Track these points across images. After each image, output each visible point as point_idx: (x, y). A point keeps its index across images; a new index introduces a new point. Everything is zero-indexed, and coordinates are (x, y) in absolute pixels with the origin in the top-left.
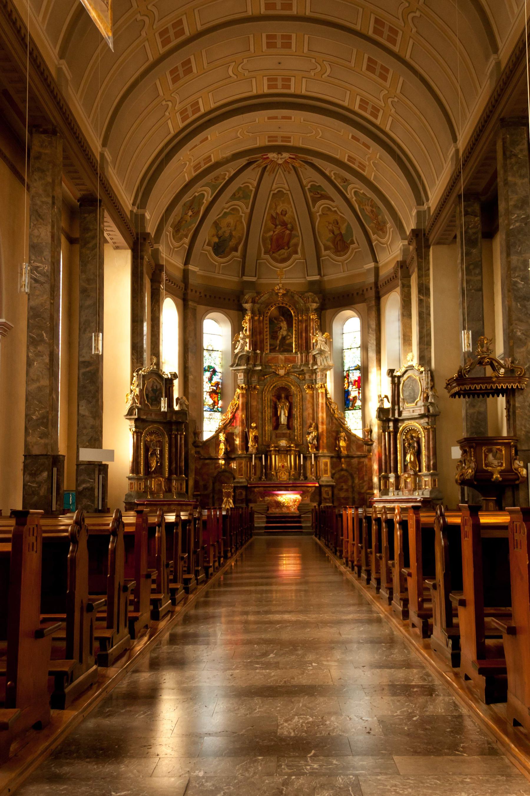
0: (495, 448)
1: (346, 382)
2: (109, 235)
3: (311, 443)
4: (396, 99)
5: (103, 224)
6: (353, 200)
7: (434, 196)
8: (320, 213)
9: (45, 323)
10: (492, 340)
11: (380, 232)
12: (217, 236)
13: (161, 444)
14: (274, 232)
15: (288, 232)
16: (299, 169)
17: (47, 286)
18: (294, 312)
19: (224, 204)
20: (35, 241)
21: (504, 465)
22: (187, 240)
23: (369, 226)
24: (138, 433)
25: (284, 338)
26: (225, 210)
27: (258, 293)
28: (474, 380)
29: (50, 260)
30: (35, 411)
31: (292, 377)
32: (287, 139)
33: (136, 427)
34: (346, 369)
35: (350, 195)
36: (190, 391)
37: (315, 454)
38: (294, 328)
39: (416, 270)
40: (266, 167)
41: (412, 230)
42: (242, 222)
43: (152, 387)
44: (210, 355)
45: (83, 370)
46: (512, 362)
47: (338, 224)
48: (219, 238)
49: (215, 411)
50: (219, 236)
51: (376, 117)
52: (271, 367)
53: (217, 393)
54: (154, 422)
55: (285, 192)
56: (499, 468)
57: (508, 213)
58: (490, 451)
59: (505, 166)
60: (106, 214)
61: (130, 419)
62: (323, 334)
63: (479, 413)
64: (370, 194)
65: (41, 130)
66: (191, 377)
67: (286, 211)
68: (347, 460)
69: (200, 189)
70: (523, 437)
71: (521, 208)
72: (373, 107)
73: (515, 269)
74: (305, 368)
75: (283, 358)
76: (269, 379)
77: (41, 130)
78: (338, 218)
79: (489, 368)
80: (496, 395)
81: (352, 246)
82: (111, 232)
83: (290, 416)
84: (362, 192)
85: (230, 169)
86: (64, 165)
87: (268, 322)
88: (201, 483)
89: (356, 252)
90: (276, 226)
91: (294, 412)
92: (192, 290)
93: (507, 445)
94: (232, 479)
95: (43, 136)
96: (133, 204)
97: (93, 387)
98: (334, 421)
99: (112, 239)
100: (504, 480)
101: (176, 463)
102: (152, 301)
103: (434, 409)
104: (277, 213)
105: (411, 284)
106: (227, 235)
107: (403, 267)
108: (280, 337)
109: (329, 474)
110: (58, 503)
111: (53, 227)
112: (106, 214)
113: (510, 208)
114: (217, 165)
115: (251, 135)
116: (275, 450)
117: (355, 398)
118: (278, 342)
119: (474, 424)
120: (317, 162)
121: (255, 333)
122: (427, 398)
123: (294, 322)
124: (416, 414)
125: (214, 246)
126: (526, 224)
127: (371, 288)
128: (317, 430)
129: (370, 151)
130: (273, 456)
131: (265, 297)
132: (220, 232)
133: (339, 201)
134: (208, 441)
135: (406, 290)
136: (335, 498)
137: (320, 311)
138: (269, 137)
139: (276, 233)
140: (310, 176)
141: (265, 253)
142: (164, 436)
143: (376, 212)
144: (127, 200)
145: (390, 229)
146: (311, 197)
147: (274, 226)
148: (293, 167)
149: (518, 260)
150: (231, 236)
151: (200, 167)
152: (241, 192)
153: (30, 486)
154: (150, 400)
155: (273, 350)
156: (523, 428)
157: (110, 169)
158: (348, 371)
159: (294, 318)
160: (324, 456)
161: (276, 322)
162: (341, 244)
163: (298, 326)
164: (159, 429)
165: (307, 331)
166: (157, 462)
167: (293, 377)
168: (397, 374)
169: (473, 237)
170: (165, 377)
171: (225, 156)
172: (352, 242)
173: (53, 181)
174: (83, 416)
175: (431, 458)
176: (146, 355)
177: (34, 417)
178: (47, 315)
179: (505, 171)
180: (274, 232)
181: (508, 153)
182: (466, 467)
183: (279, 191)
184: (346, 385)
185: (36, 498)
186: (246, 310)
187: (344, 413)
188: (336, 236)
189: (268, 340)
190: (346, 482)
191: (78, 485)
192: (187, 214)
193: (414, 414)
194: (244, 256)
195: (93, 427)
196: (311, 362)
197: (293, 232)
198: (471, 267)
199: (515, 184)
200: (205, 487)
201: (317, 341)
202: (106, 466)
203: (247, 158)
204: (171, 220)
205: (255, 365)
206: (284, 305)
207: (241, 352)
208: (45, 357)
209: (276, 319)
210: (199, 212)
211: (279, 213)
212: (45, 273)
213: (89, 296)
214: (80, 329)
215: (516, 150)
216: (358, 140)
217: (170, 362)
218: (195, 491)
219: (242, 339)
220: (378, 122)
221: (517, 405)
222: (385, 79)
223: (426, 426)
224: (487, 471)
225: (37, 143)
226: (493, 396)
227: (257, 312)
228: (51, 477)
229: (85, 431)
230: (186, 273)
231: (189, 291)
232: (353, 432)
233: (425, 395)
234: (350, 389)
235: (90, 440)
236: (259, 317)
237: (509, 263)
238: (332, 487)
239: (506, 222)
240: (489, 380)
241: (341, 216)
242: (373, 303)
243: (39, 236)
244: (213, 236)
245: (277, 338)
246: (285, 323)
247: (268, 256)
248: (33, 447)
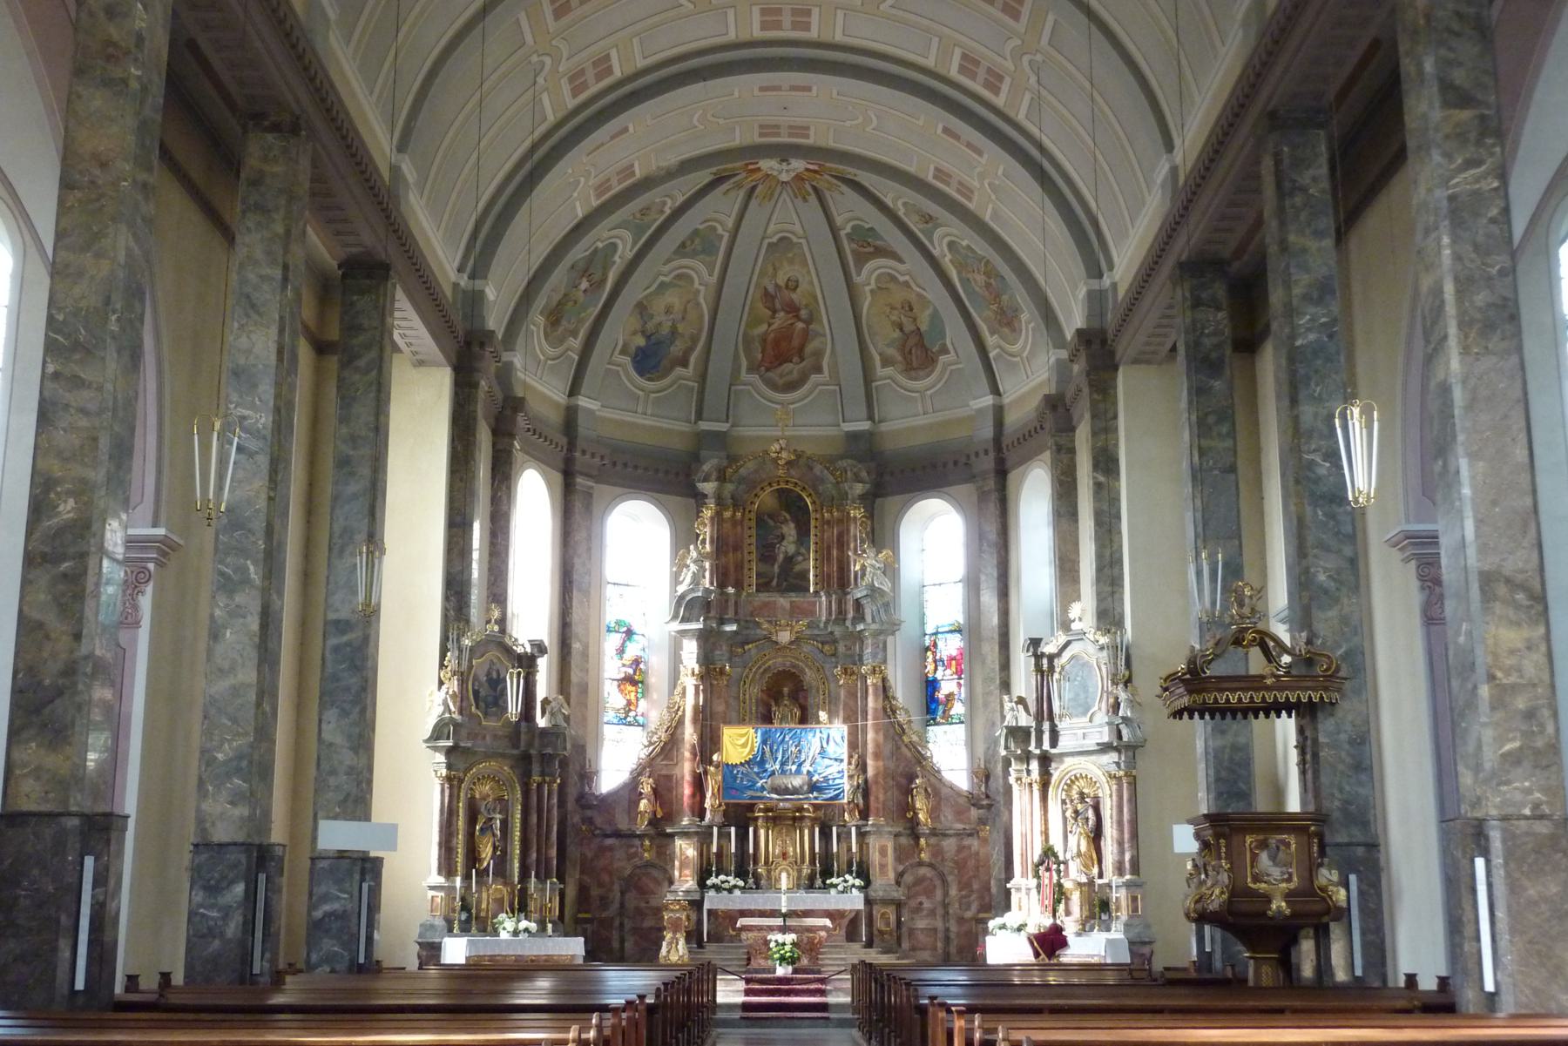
0: (1273, 840)
1: (930, 659)
2: (403, 336)
4: (1039, 57)
5: (392, 314)
6: (947, 261)
7: (1126, 258)
8: (873, 286)
9: (255, 543)
10: (1261, 591)
11: (1006, 330)
12: (643, 332)
13: (503, 804)
16: (827, 194)
17: (263, 461)
18: (813, 503)
19: (659, 265)
20: (242, 361)
21: (1295, 879)
22: (576, 343)
24: (452, 782)
25: (789, 560)
26: (662, 278)
27: (733, 459)
28: (1223, 683)
29: (271, 404)
30: (222, 741)
31: (806, 648)
32: (803, 130)
33: (449, 767)
34: (929, 629)
35: (939, 249)
37: (858, 827)
38: (812, 538)
39: (1087, 416)
40: (753, 188)
41: (1078, 331)
42: (698, 304)
43: (488, 674)
45: (333, 641)
46: (1309, 642)
48: (648, 338)
49: (630, 724)
51: (996, 90)
52: (758, 625)
53: (634, 683)
54: (488, 756)
55: (795, 240)
56: (1284, 885)
57: (1290, 312)
58: (1263, 845)
59: (1281, 211)
60: (400, 294)
61: (436, 749)
62: (879, 552)
63: (1235, 748)
64: (982, 248)
65: (266, 123)
68: (933, 840)
69: (606, 234)
70: (1336, 815)
71: (1320, 301)
72: (989, 71)
73: (1310, 434)
74: (838, 631)
75: (788, 606)
76: (753, 652)
77: (266, 123)
78: (913, 298)
79: (1255, 653)
80: (1273, 714)
81: (943, 359)
82: (409, 327)
84: (964, 243)
85: (676, 192)
86: (313, 194)
87: (753, 524)
88: (595, 892)
90: (774, 312)
93: (1302, 830)
95: (270, 137)
96: (460, 270)
97: (354, 680)
98: (904, 750)
99: (409, 345)
100: (1294, 915)
101: (538, 851)
102: (493, 478)
103: (1133, 732)
104: (777, 286)
105: (1077, 443)
106: (665, 330)
107: (1057, 408)
108: (781, 557)
109: (891, 875)
110: (267, 955)
111: (281, 331)
112: (400, 294)
113: (1295, 302)
114: (647, 184)
115: (721, 121)
116: (767, 819)
117: (950, 697)
118: (776, 569)
119: (1224, 774)
120: (866, 178)
121: (723, 546)
122: (1116, 707)
123: (813, 523)
124: (1091, 743)
126: (1331, 336)
127: (986, 452)
128: (864, 771)
129: (983, 160)
130: (762, 832)
131: (747, 468)
132: (650, 326)
133: (913, 262)
134: (614, 794)
135: (1065, 457)
136: (904, 929)
137: (870, 500)
138: (761, 126)
140: (850, 209)
141: (750, 370)
142: (513, 788)
143: (995, 289)
144: (444, 257)
145: (1028, 323)
146: (853, 251)
148: (815, 189)
149: (1316, 415)
150: (674, 332)
151: (609, 189)
152: (697, 241)
153: (203, 915)
154: (482, 704)
155: (764, 586)
156: (1337, 795)
157: (412, 197)
158: (936, 634)
159: (813, 515)
161: (771, 523)
162: (919, 353)
163: (823, 532)
165: (842, 544)
166: (495, 848)
168: (1049, 648)
169: (1214, 355)
170: (520, 650)
171: (664, 164)
172: (944, 351)
173: (288, 232)
174: (331, 744)
175: (1126, 846)
176: (476, 596)
177: (220, 756)
178: (259, 525)
179: (1282, 224)
181: (1287, 184)
182: (1209, 883)
183: (781, 239)
184: (930, 667)
185: (217, 943)
186: (705, 496)
187: (926, 732)
188: (907, 336)
190: (929, 893)
191: (312, 907)
192: (577, 290)
193: (1087, 742)
194: (703, 377)
195: (351, 771)
196: (851, 615)
198: (1211, 419)
199: (1304, 251)
200: (604, 902)
201: (863, 568)
202: (378, 862)
203: (714, 170)
204: (541, 302)
205: (722, 622)
206: (790, 486)
207: (692, 590)
208: (249, 618)
209: (771, 516)
210: (603, 281)
212: (258, 431)
213: (352, 474)
214: (330, 549)
215: (1305, 178)
216: (957, 137)
217: (530, 615)
218: (579, 911)
219: (695, 562)
220: (1000, 101)
221: (1322, 739)
222: (1016, 16)
223: (1113, 769)
224: (1255, 894)
225: (258, 151)
226: (1267, 716)
227: (730, 501)
228: (251, 894)
229: (332, 781)
230: (570, 419)
231: (577, 454)
232: (947, 776)
233: (1111, 700)
234: (939, 675)
235: (345, 800)
237: (1296, 420)
238: (899, 905)
239: (1287, 330)
240: (1255, 683)
241: (919, 295)
243: (249, 352)
244: (634, 333)
246: (792, 525)
247: (755, 378)
248: (213, 824)
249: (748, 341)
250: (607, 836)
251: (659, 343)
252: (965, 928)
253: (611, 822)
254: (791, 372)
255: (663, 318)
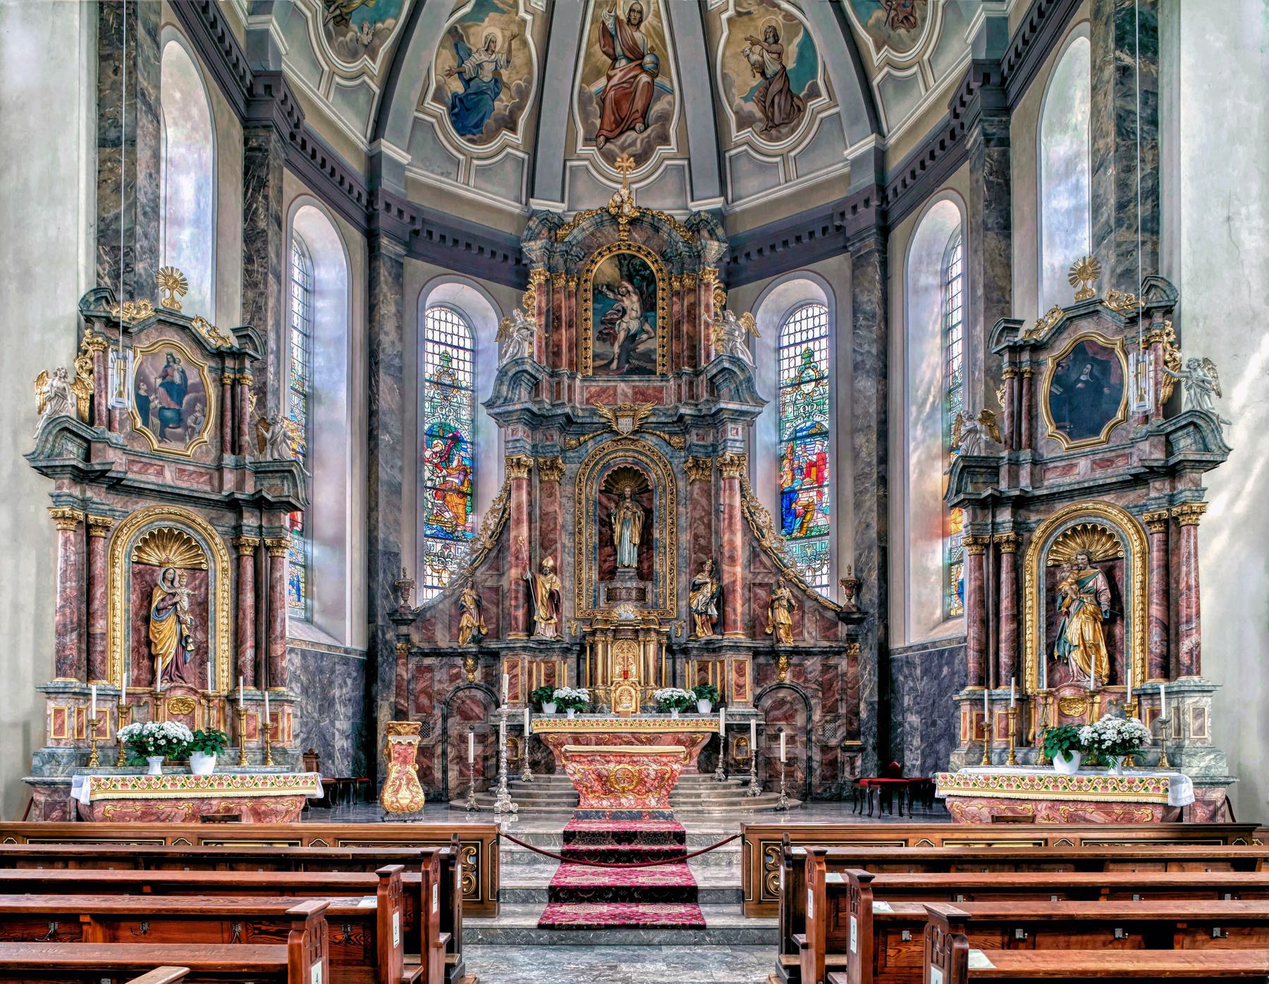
3: (700, 614)
8: (731, 12)
14: (609, 78)
15: (644, 78)
22: (376, 67)
23: (865, 27)
36: (383, 475)
42: (525, 43)
44: (446, 398)
47: (776, 42)
48: (467, 83)
50: (467, 77)
66: (385, 438)
67: (641, 12)
75: (630, 392)
81: (813, 104)
83: (646, 544)
87: (590, 295)
89: (822, 120)
91: (656, 535)
92: (388, 206)
94: (493, 707)
101: (257, 647)
104: (617, 18)
106: (487, 76)
108: (622, 335)
109: (749, 697)
118: (616, 349)
125: (454, 107)
127: (867, 202)
139: (615, 81)
147: (610, 61)
160: (736, 648)
161: (611, 295)
164: (190, 523)
167: (654, 439)
180: (609, 78)
189: (590, 343)
190: (789, 717)
197: (658, 80)
211: (623, 17)
230: (374, 162)
236: (567, 282)
241: (789, 16)
242: (871, 242)
244: (449, 74)
245: (615, 338)
246: (635, 298)
247: (592, 150)
249: (584, 101)
250: (426, 655)
251: (480, 93)
252: (830, 756)
253: (430, 639)
254: (633, 143)
255: (484, 57)
